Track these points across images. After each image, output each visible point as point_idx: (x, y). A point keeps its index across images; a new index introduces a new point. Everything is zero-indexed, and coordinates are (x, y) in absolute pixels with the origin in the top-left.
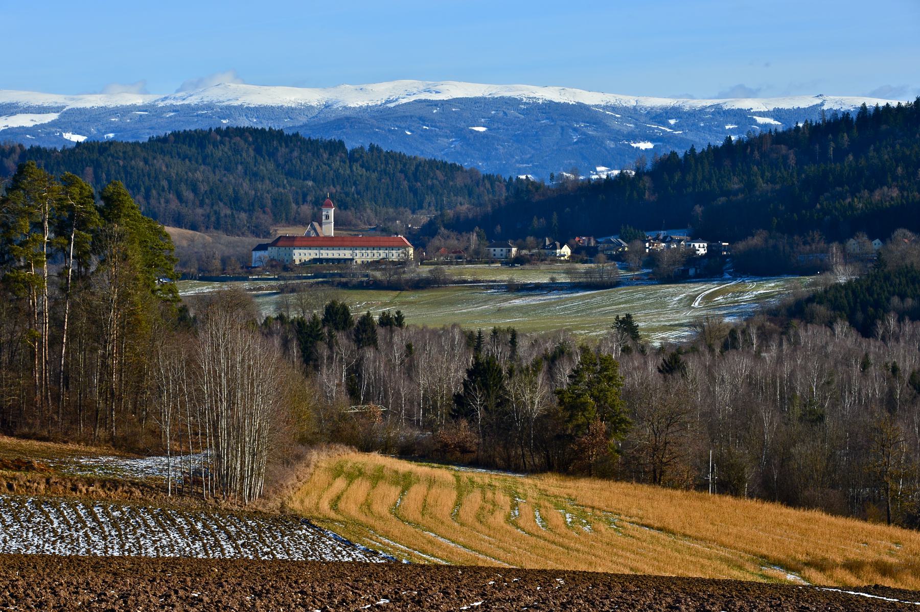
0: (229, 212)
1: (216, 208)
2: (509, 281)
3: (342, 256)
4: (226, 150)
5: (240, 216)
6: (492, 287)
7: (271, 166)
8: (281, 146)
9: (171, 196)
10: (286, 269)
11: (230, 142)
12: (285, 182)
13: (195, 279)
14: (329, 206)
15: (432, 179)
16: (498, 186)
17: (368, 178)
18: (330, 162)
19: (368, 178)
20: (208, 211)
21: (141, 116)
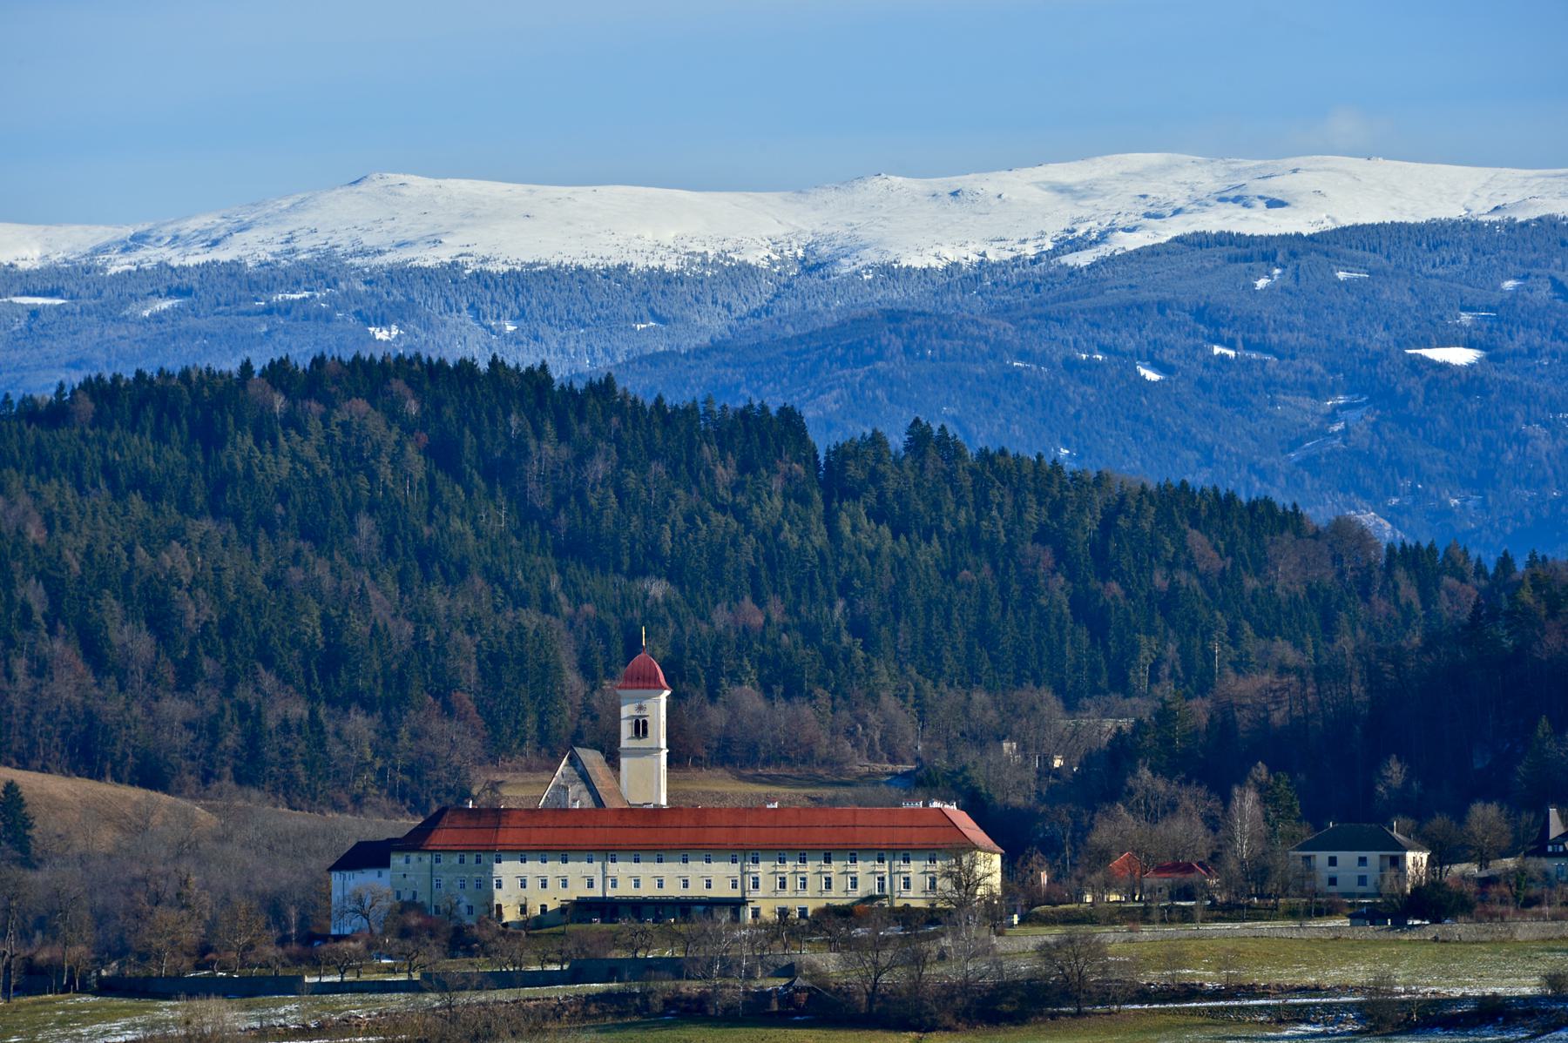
0: (298, 710)
1: (244, 692)
2: (1375, 989)
3: (697, 890)
4: (309, 451)
5: (348, 727)
6: (1300, 1015)
7: (497, 518)
8: (539, 434)
9: (58, 645)
10: (461, 942)
11: (325, 420)
12: (555, 583)
13: (84, 989)
14: (647, 683)
15: (1171, 566)
16: (1451, 594)
17: (900, 564)
18: (741, 499)
19: (900, 564)
20: (211, 707)
21: (34, 313)
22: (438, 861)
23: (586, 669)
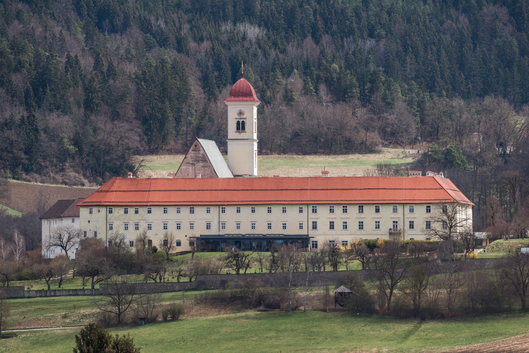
22: (111, 212)
23: (205, 81)
